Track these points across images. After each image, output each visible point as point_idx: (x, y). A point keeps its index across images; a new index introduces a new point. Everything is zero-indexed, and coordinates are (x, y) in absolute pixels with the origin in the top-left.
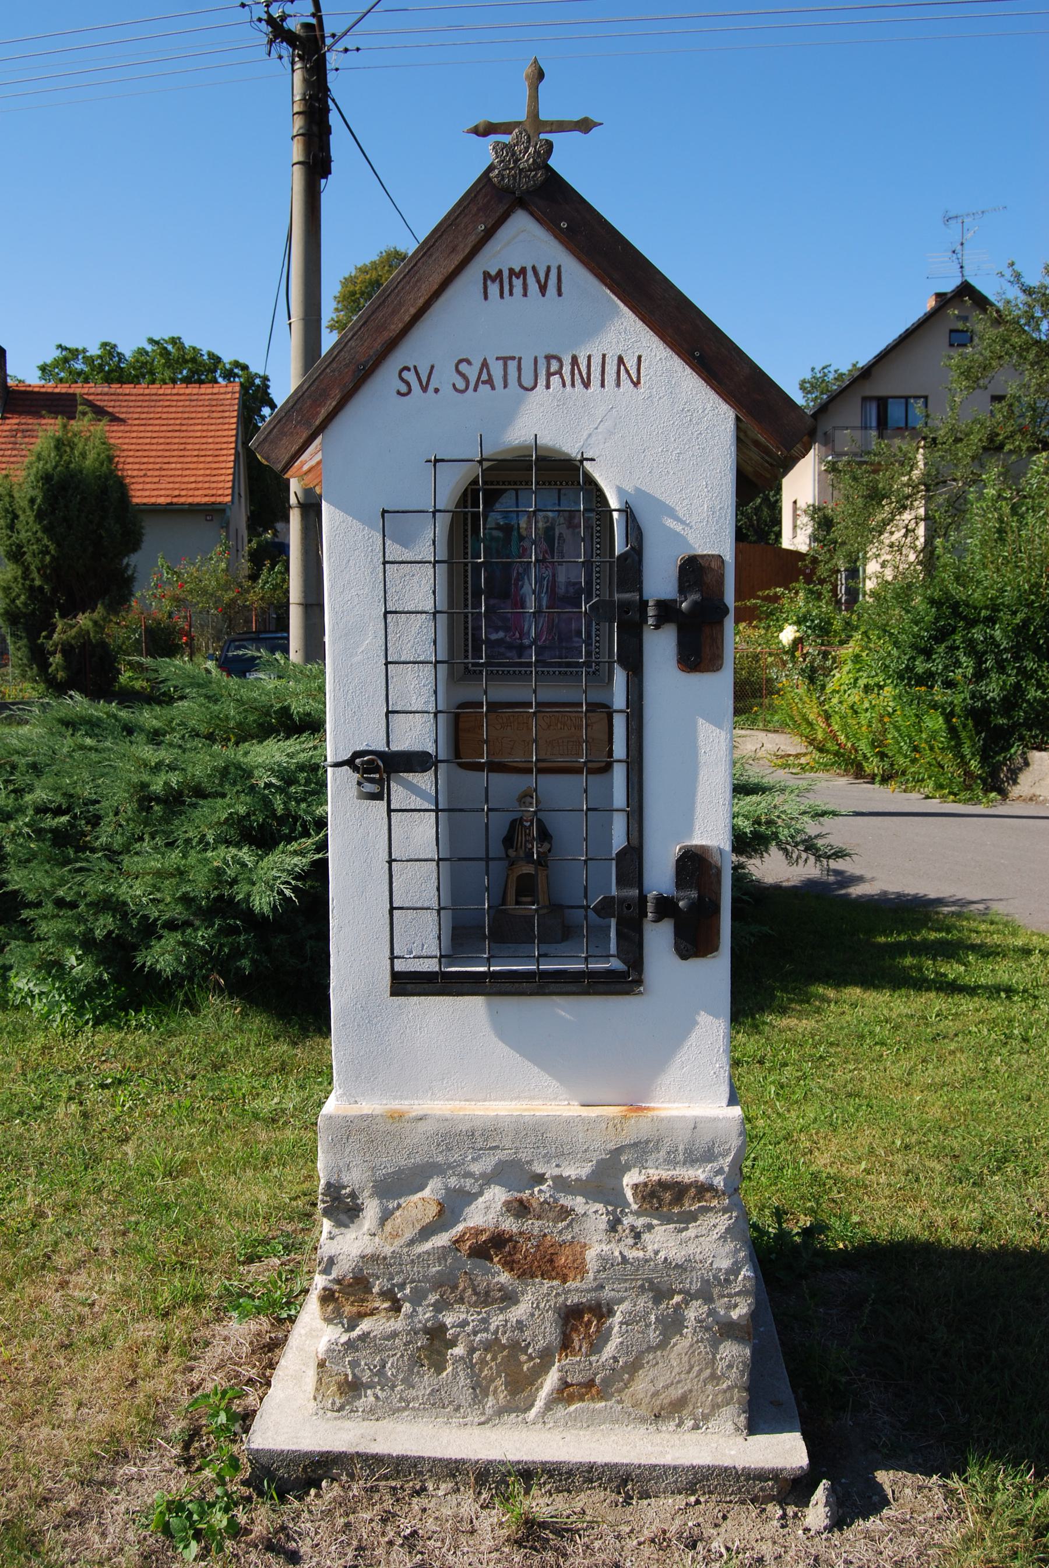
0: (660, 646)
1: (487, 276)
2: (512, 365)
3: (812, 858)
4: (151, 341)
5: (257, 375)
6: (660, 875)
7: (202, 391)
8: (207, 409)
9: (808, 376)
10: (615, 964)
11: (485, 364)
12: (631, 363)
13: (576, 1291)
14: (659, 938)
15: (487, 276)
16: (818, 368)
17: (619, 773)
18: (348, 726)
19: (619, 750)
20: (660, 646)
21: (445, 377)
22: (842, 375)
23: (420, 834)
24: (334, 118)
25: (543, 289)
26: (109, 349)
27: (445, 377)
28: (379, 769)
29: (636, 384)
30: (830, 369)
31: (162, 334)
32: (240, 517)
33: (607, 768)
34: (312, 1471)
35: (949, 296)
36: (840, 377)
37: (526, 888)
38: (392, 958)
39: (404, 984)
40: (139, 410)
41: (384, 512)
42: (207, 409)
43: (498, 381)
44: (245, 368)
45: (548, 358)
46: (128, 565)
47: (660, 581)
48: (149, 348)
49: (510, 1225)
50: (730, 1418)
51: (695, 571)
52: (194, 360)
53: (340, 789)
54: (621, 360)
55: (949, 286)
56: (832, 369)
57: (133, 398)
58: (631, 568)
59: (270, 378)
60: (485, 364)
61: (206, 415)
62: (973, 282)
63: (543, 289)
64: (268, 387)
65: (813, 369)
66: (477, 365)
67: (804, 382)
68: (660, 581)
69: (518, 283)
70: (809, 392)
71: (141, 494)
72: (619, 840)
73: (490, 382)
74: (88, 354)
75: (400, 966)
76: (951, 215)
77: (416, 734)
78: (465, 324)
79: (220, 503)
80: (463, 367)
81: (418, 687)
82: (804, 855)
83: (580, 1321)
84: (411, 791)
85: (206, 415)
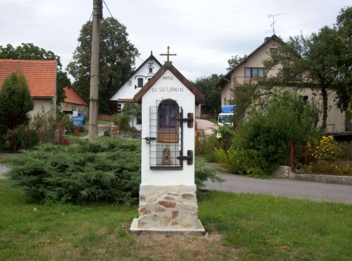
0: (185, 125)
1: (164, 77)
2: (167, 89)
3: (218, 181)
4: (23, 44)
5: (56, 56)
6: (185, 154)
7: (45, 62)
8: (47, 68)
9: (231, 59)
10: (179, 166)
11: (163, 88)
12: (182, 89)
13: (174, 209)
14: (185, 163)
15: (164, 77)
16: (234, 57)
17: (180, 141)
18: (145, 134)
19: (180, 137)
20: (185, 125)
21: (158, 90)
22: (241, 58)
23: (154, 149)
24: (103, 5)
25: (171, 79)
26: (9, 47)
27: (158, 90)
28: (149, 140)
29: (182, 91)
30: (238, 56)
31: (26, 42)
32: (55, 100)
33: (178, 142)
34: (139, 233)
35: (270, 38)
36: (241, 59)
37: (167, 158)
38: (150, 164)
39: (152, 168)
40: (26, 68)
41: (150, 107)
42: (47, 68)
43: (165, 90)
44: (52, 53)
45: (171, 88)
46: (29, 114)
47: (185, 116)
48: (22, 46)
49: (166, 200)
50: (195, 226)
51: (190, 115)
52: (36, 51)
53: (144, 142)
54: (180, 88)
55: (270, 35)
56: (238, 57)
57: (24, 64)
58: (181, 114)
59: (61, 57)
60: (163, 88)
61: (46, 70)
62: (278, 35)
63: (171, 79)
64: (59, 60)
65: (232, 56)
66: (162, 88)
67: (229, 60)
68: (185, 116)
69: (167, 78)
70: (231, 64)
71: (34, 93)
72: (180, 149)
73: (164, 91)
74: (2, 48)
75: (151, 166)
76: (270, 15)
77: (154, 135)
78: (161, 83)
79: (51, 97)
80: (161, 89)
81: (155, 129)
82: (216, 180)
83: (175, 214)
84: (154, 143)
85: (46, 70)
